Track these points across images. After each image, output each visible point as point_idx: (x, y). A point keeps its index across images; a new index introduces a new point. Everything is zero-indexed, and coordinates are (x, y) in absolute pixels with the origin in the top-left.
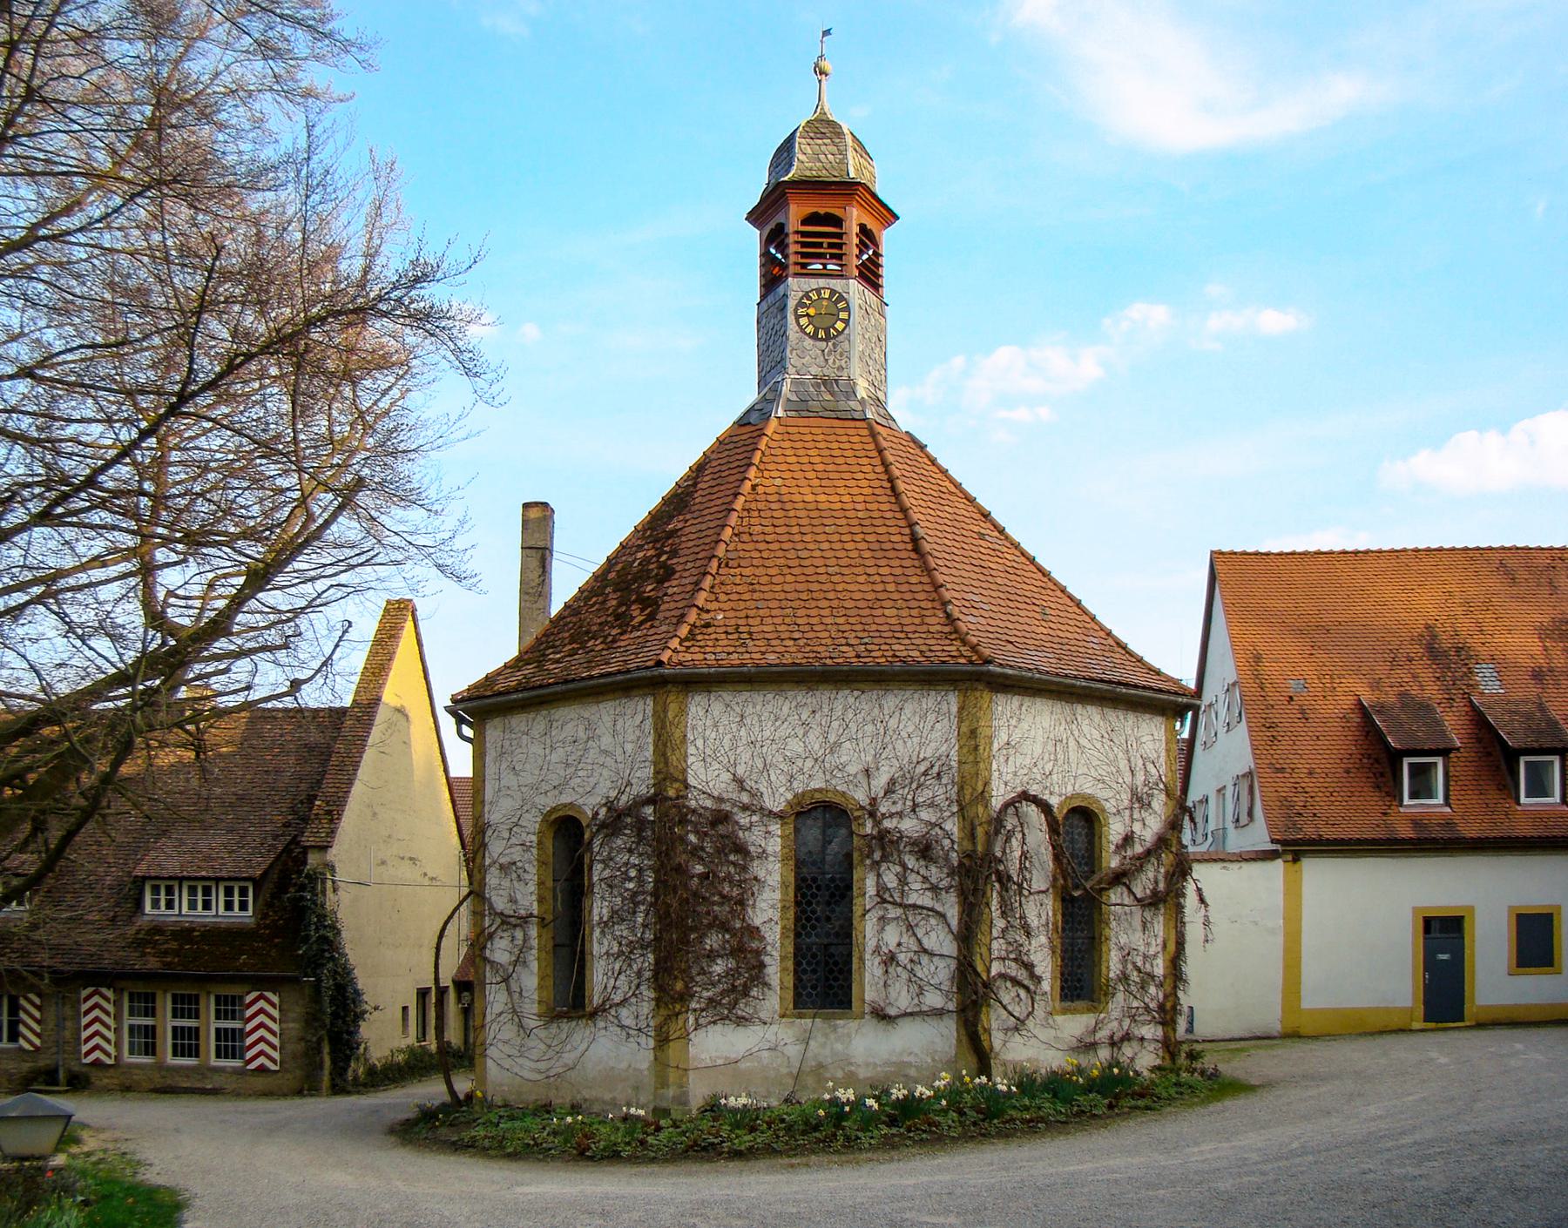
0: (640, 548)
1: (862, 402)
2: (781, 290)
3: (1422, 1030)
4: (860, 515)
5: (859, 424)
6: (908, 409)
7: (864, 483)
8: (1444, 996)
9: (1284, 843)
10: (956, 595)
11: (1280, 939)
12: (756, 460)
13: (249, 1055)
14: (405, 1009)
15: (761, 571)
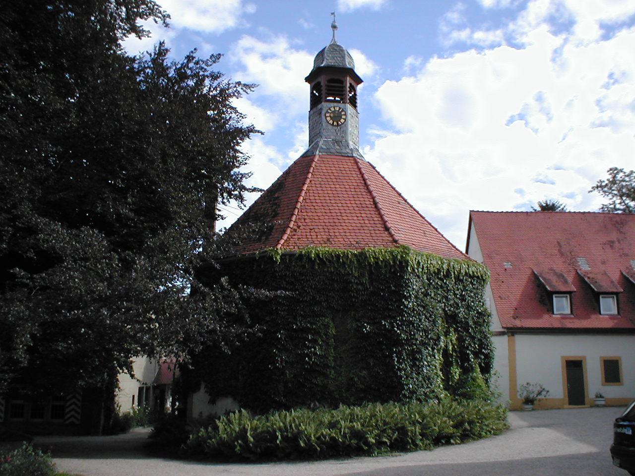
0: (263, 204)
1: (351, 150)
2: (319, 106)
3: (567, 408)
4: (353, 193)
5: (350, 158)
6: (368, 155)
7: (353, 181)
8: (576, 392)
9: (508, 328)
10: (392, 225)
11: (508, 369)
12: (311, 171)
13: (66, 417)
14: (134, 396)
15: (315, 214)
